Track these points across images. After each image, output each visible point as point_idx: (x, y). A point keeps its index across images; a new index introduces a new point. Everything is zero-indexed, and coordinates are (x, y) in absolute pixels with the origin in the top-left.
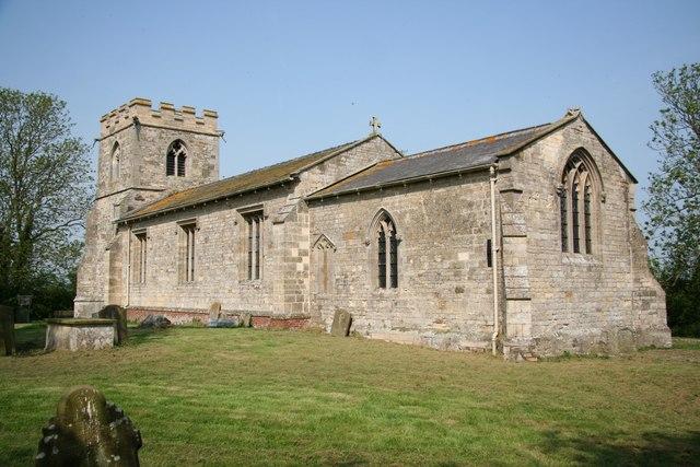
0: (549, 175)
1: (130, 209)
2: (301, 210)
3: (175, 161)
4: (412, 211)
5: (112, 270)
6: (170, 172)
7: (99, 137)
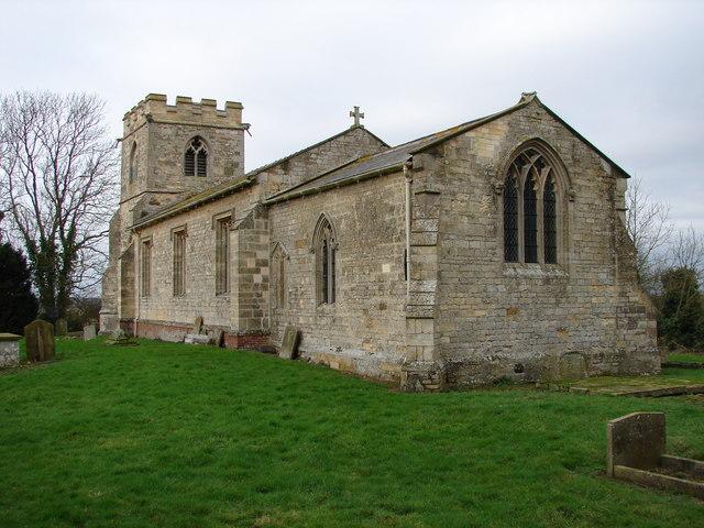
0: (485, 172)
1: (144, 214)
2: (258, 216)
3: (195, 161)
4: (346, 217)
5: (125, 280)
6: (189, 171)
7: (122, 136)
